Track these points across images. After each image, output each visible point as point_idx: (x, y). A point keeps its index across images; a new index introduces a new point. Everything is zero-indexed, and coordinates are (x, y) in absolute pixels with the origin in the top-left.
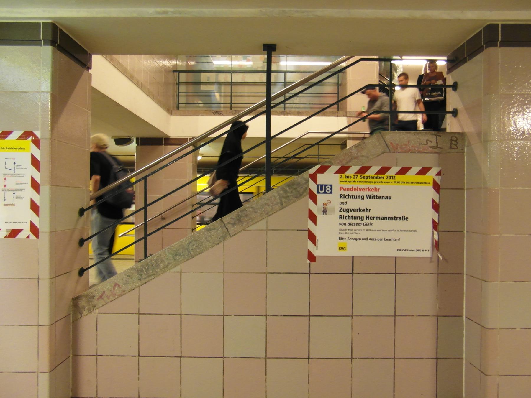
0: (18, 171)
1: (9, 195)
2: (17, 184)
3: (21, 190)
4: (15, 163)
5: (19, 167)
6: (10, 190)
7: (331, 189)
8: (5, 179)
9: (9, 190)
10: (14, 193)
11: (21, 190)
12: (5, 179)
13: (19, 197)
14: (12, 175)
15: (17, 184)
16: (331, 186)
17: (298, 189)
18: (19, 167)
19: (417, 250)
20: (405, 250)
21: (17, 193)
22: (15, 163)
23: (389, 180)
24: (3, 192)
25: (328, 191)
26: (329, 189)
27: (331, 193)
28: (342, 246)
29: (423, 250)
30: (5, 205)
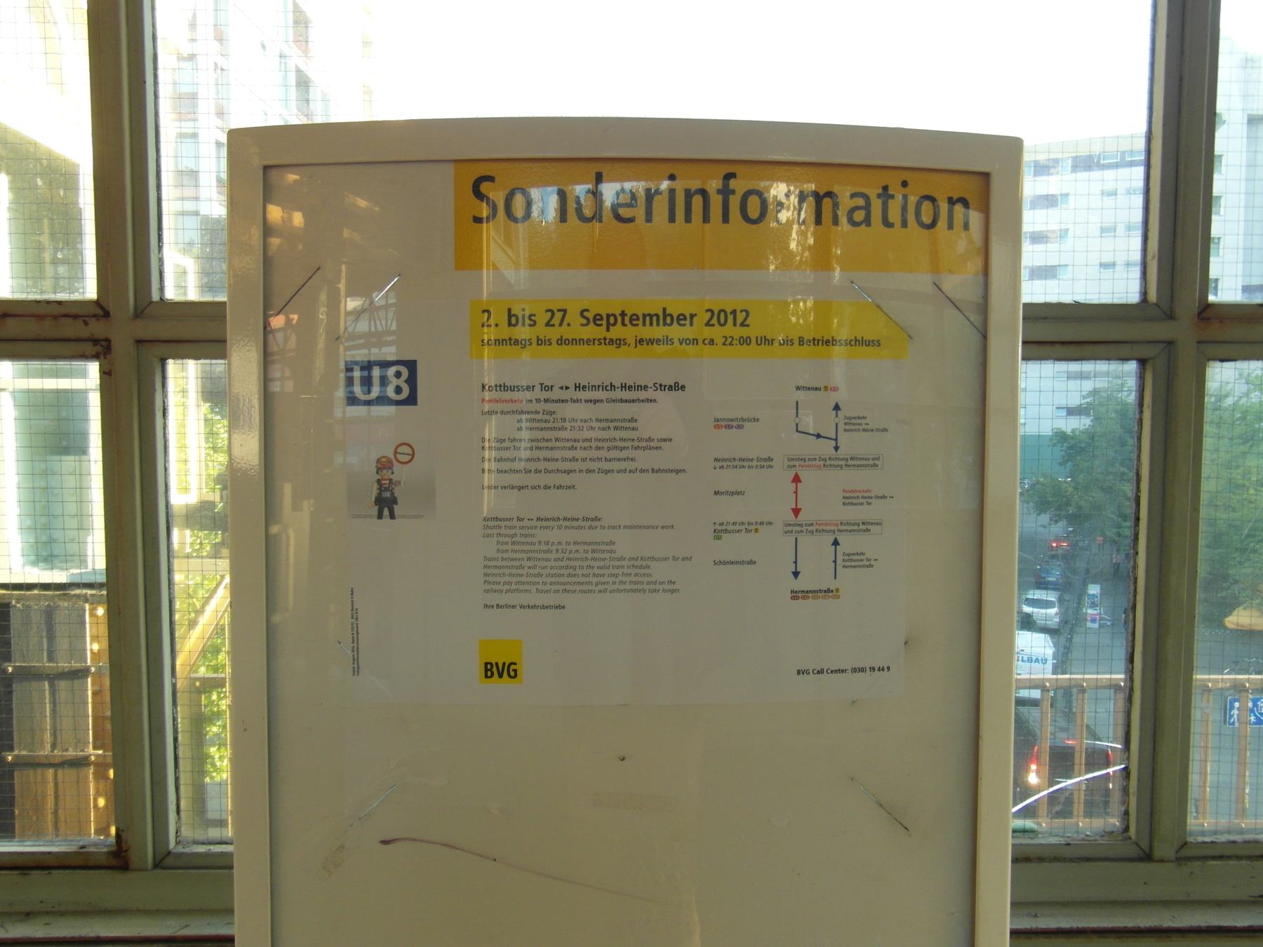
0: (852, 444)
1: (815, 551)
2: (850, 499)
3: (864, 527)
4: (837, 408)
5: (855, 424)
6: (817, 529)
7: (412, 381)
8: (797, 479)
9: (817, 529)
10: (836, 543)
11: (864, 527)
12: (797, 479)
13: (857, 561)
14: (826, 463)
15: (850, 499)
16: (411, 365)
17: (1226, 441)
18: (855, 424)
19: (854, 670)
20: (820, 672)
21: (849, 543)
22: (837, 408)
23: (717, 332)
24: (792, 539)
25: (398, 390)
26: (401, 382)
27: (412, 400)
28: (500, 658)
29: (873, 669)
30: (795, 595)
